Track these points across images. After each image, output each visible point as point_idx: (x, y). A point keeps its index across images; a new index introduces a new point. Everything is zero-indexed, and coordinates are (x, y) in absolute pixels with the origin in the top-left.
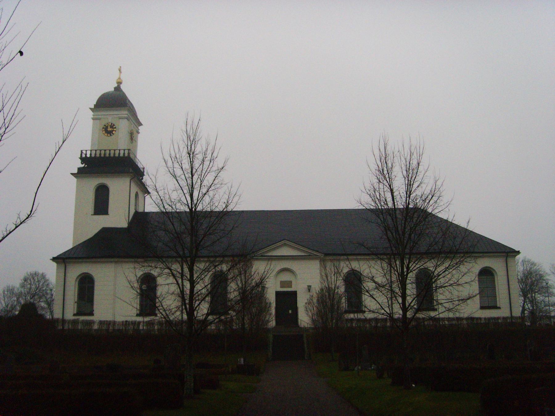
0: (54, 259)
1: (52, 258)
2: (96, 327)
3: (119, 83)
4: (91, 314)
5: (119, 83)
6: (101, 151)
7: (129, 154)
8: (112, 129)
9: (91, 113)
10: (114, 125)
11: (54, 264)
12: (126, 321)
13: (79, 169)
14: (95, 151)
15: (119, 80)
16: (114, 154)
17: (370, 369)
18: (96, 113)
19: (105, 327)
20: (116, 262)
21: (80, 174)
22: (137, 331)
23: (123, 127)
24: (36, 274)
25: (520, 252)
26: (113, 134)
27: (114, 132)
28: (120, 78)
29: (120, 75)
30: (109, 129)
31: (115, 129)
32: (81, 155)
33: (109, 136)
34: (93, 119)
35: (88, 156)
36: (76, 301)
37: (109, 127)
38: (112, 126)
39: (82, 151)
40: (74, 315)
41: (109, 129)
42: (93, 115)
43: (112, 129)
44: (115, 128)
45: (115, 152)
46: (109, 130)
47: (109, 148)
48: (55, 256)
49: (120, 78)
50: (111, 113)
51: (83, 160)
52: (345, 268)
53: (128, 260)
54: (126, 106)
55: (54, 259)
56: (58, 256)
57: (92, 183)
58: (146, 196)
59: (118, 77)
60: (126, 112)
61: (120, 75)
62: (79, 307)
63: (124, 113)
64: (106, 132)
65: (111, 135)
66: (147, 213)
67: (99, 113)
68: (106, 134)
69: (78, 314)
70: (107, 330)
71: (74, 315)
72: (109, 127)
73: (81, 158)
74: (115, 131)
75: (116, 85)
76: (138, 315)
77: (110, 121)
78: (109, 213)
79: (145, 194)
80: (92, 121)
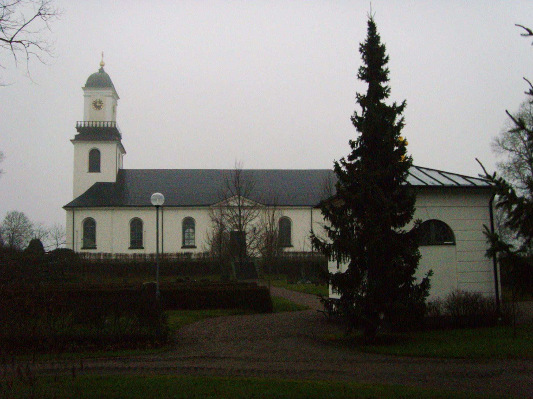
0: (65, 207)
1: (63, 206)
2: (114, 258)
3: (102, 65)
4: (94, 248)
5: (102, 65)
6: (92, 122)
7: (115, 125)
8: (100, 105)
9: (83, 91)
10: (101, 101)
11: (65, 212)
12: (135, 254)
13: (76, 136)
14: (99, 122)
15: (102, 64)
16: (107, 125)
17: (306, 283)
18: (86, 91)
19: (180, 258)
20: (112, 209)
21: (77, 139)
22: (99, 260)
23: (108, 102)
24: (22, 215)
25: (351, 140)
26: (101, 108)
27: (102, 107)
28: (102, 62)
29: (103, 59)
30: (98, 104)
31: (102, 105)
32: (77, 124)
33: (98, 110)
34: (85, 96)
35: (83, 126)
36: (82, 238)
37: (98, 103)
38: (100, 102)
39: (77, 122)
40: (82, 249)
41: (98, 104)
42: (85, 93)
43: (100, 105)
44: (103, 104)
45: (89, 123)
46: (98, 105)
47: (96, 120)
48: (65, 205)
49: (102, 62)
50: (99, 91)
51: (79, 129)
52: (278, 215)
53: (122, 208)
54: (110, 86)
55: (65, 207)
56: (67, 205)
57: (87, 148)
58: (123, 156)
59: (100, 61)
60: (111, 91)
61: (103, 59)
62: (84, 243)
63: (109, 92)
64: (97, 108)
65: (99, 109)
66: (124, 170)
67: (90, 92)
68: (95, 108)
69: (83, 248)
70: (204, 258)
71: (82, 249)
72: (98, 103)
73: (77, 128)
74: (103, 106)
75: (100, 67)
76: (130, 248)
77: (98, 98)
78: (101, 171)
79: (122, 154)
80: (83, 97)
